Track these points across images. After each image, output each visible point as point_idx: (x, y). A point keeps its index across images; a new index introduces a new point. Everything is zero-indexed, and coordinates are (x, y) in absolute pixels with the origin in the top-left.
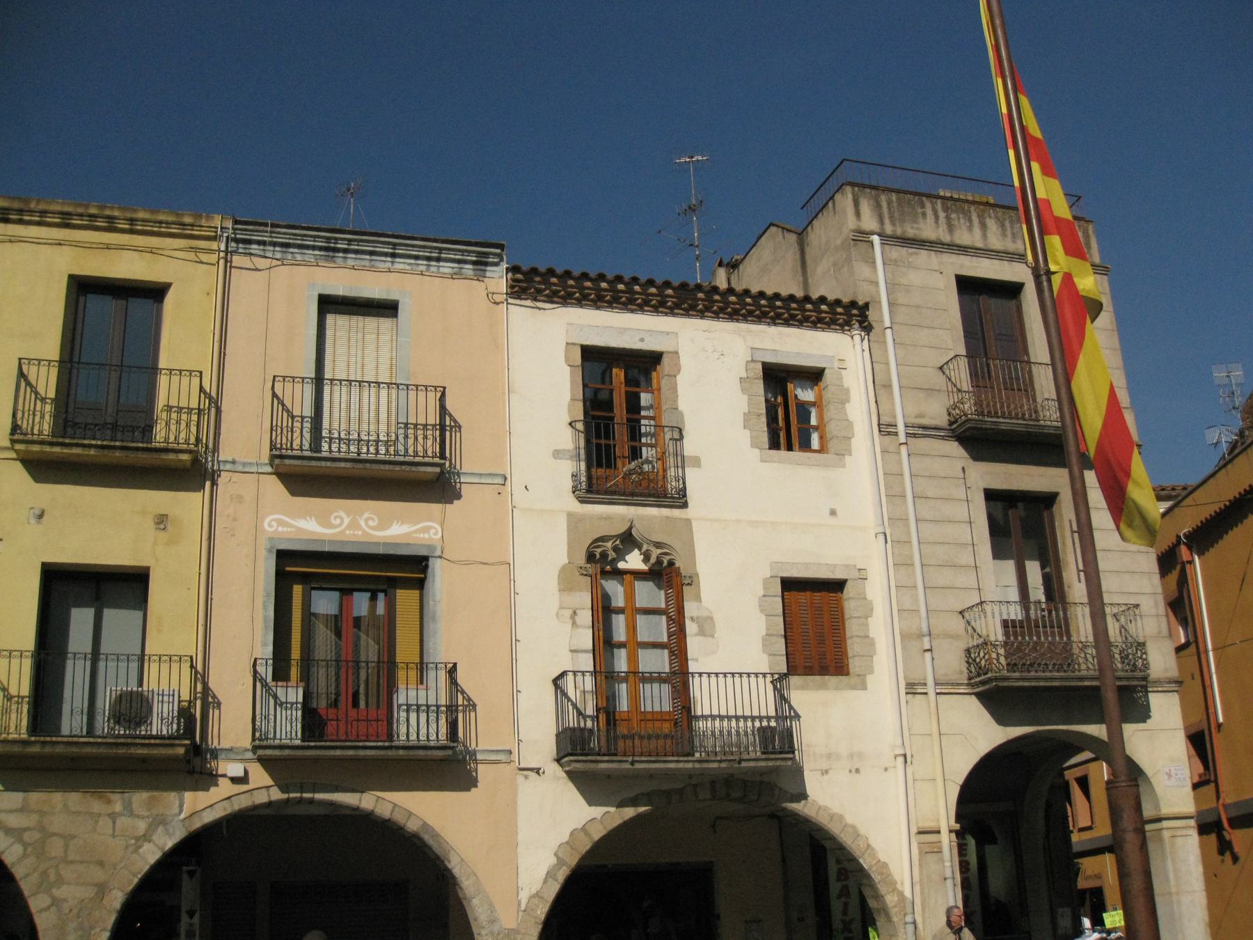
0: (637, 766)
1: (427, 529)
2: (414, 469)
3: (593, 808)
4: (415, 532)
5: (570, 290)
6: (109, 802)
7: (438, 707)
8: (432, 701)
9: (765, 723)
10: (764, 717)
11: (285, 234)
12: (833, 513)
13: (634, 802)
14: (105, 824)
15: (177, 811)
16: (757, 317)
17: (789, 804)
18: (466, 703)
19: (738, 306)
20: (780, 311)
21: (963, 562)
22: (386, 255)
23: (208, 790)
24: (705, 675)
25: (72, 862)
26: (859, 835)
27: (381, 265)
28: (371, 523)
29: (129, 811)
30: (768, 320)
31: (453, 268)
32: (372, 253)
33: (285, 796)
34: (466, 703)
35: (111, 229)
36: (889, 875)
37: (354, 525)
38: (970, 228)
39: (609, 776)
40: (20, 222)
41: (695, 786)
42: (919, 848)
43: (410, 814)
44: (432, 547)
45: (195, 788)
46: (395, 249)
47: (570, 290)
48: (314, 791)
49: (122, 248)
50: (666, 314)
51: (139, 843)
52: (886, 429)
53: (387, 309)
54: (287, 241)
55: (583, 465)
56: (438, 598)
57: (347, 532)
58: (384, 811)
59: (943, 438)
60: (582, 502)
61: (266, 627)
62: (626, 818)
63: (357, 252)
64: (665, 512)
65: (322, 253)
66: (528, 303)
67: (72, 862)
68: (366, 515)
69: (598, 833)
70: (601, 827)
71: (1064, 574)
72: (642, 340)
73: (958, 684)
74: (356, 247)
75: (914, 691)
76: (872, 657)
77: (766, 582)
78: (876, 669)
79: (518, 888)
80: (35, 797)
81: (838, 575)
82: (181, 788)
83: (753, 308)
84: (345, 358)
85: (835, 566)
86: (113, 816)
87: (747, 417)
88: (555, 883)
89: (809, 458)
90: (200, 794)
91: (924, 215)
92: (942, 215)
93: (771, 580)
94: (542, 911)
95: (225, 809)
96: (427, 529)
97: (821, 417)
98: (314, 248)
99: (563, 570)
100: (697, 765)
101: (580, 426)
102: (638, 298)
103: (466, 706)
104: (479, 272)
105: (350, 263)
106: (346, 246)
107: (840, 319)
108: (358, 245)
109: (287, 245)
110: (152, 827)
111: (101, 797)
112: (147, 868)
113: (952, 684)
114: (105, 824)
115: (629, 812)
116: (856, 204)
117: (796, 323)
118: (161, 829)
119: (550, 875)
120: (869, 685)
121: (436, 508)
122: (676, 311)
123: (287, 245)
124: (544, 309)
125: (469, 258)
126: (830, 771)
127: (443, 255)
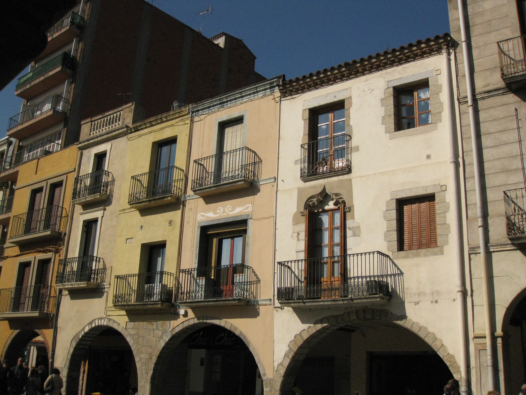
1: (247, 208)
2: (235, 184)
3: (304, 324)
4: (243, 210)
5: (302, 85)
9: (368, 279)
10: (364, 277)
11: (207, 103)
12: (428, 157)
13: (321, 322)
15: (168, 327)
16: (390, 64)
17: (396, 322)
18: (257, 280)
19: (378, 63)
20: (409, 54)
21: (514, 167)
22: (240, 98)
23: (256, 318)
24: (293, 262)
25: (144, 346)
26: (436, 339)
28: (229, 209)
30: (397, 64)
31: (263, 93)
34: (257, 280)
35: (163, 122)
36: (456, 362)
37: (224, 211)
39: (310, 309)
40: (142, 129)
41: (349, 313)
42: (475, 347)
43: (236, 328)
44: (248, 215)
45: (173, 320)
46: (241, 94)
47: (302, 85)
49: (165, 128)
50: (347, 80)
51: (160, 339)
53: (239, 120)
54: (208, 106)
55: (306, 165)
56: (249, 236)
57: (222, 215)
58: (228, 327)
59: (503, 94)
60: (305, 182)
61: (196, 257)
62: (318, 329)
63: (231, 100)
64: (341, 177)
65: (220, 105)
66: (289, 97)
68: (228, 206)
69: (306, 336)
70: (307, 334)
72: (335, 97)
73: (505, 245)
74: (229, 99)
75: (475, 252)
76: (448, 235)
77: (388, 203)
78: (450, 242)
79: (274, 360)
80: (137, 323)
81: (429, 191)
82: (170, 320)
83: (386, 61)
84: (230, 144)
85: (427, 187)
86: (154, 330)
87: (383, 118)
88: (288, 359)
89: (416, 130)
90: (175, 321)
93: (391, 201)
94: (282, 371)
95: (182, 327)
96: (247, 208)
98: (217, 105)
99: (295, 215)
100: (333, 303)
101: (306, 147)
102: (331, 78)
103: (257, 281)
104: (272, 92)
105: (229, 105)
106: (226, 100)
107: (434, 48)
108: (230, 98)
111: (151, 323)
112: (161, 348)
113: (501, 245)
114: (152, 332)
115: (319, 326)
117: (412, 59)
119: (286, 355)
120: (445, 252)
121: (250, 198)
122: (351, 77)
123: (209, 107)
124: (295, 98)
125: (267, 87)
126: (419, 302)
127: (258, 90)
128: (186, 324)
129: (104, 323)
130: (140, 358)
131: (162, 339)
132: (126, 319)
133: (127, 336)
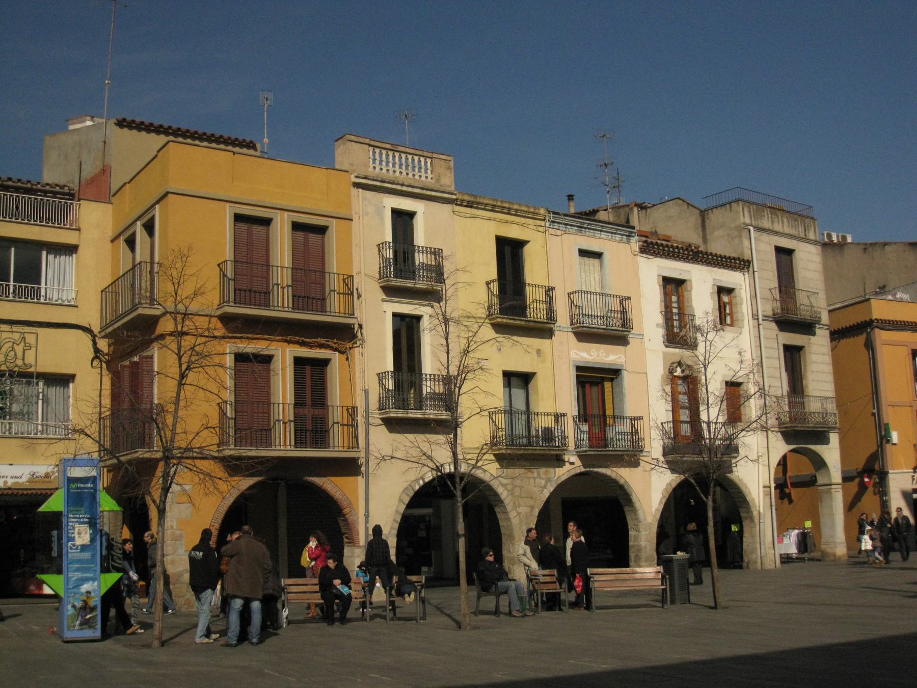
0: (685, 459)
6: (533, 473)
7: (627, 433)
8: (623, 431)
14: (532, 481)
15: (553, 476)
17: (310, 478)
22: (598, 230)
25: (523, 497)
27: (597, 235)
29: (539, 476)
32: (594, 230)
33: (585, 470)
37: (598, 355)
38: (778, 222)
40: (477, 208)
45: (559, 467)
48: (593, 468)
52: (755, 317)
58: (614, 476)
59: (771, 321)
67: (523, 497)
68: (602, 351)
71: (804, 381)
82: (555, 466)
86: (534, 478)
91: (764, 216)
92: (770, 216)
97: (731, 309)
98: (575, 226)
101: (663, 313)
109: (566, 224)
110: (546, 483)
114: (532, 481)
115: (318, 481)
116: (743, 209)
118: (549, 483)
119: (661, 501)
128: (573, 472)
129: (450, 469)
130: (518, 512)
131: (546, 488)
132: (497, 465)
133: (498, 487)
